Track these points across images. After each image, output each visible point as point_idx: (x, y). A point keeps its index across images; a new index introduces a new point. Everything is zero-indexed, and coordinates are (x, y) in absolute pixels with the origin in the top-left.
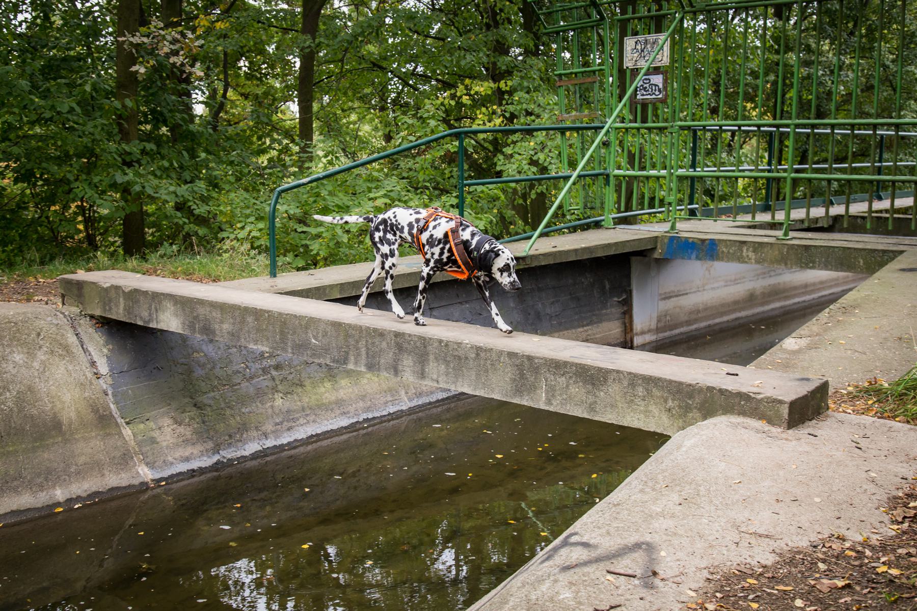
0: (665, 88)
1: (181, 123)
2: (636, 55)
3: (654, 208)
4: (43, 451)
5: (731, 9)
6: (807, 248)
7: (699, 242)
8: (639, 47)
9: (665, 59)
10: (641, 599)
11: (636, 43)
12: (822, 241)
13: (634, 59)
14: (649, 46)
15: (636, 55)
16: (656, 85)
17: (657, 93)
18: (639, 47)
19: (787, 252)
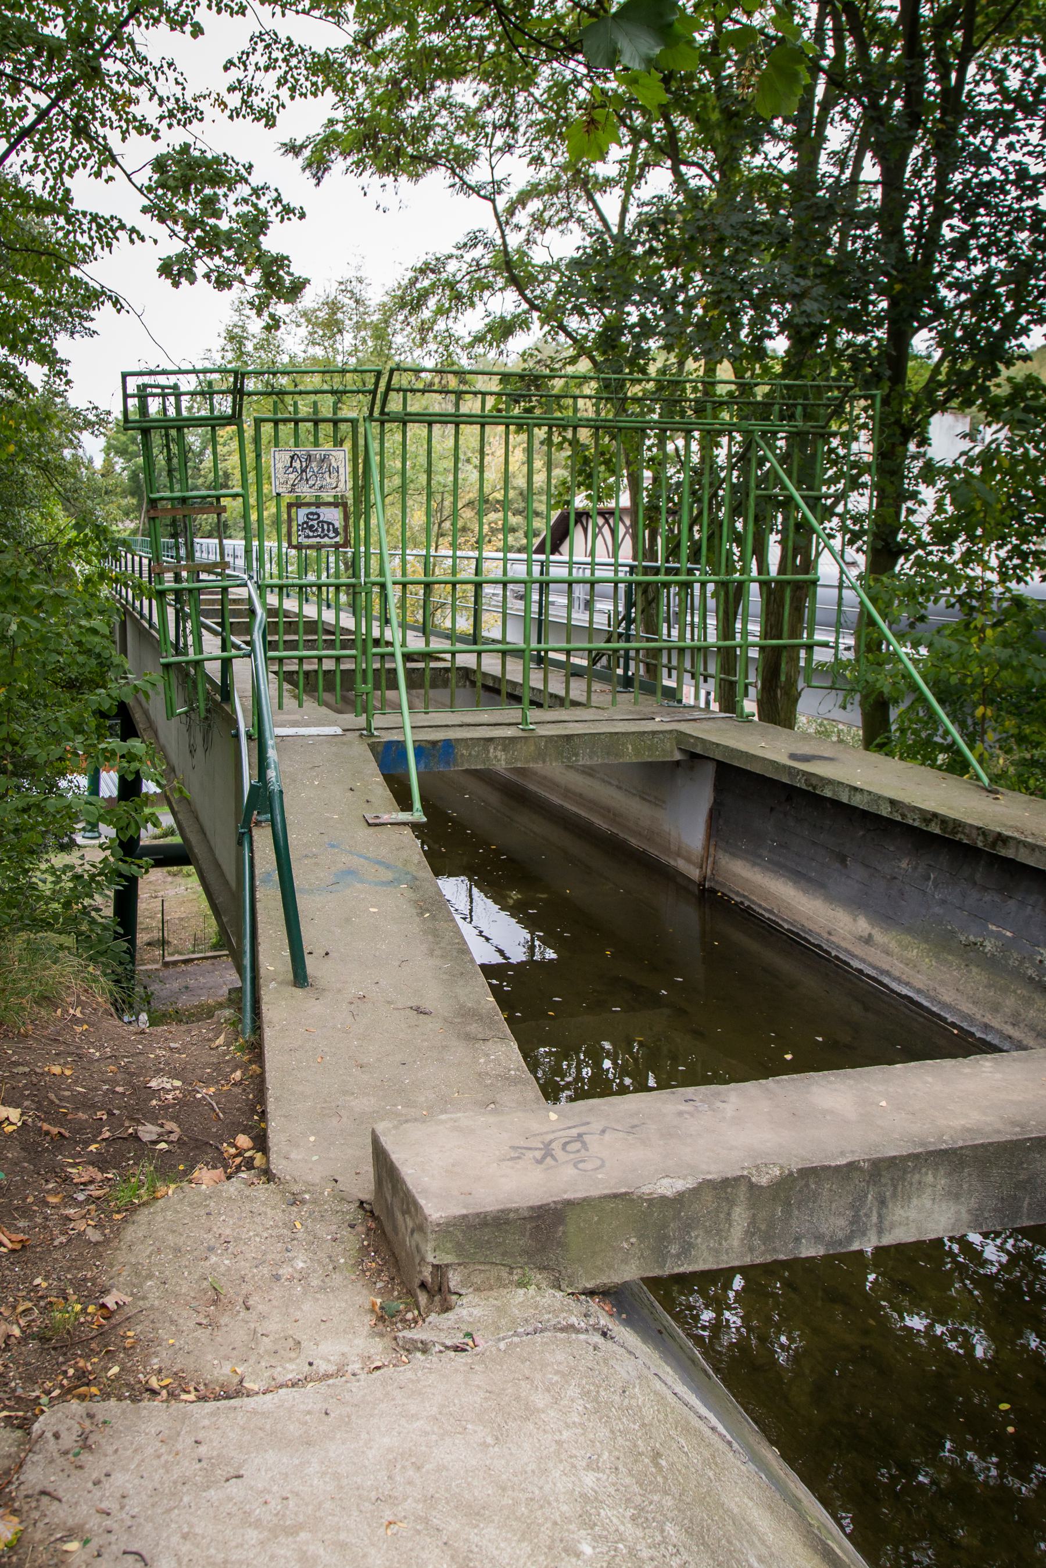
0: (346, 528)
1: (922, 450)
2: (292, 476)
3: (780, 638)
4: (315, 1238)
5: (539, 426)
6: (569, 738)
7: (429, 746)
8: (297, 464)
9: (341, 485)
10: (109, 1532)
11: (292, 458)
12: (587, 725)
13: (290, 482)
14: (314, 464)
15: (292, 476)
16: (329, 523)
17: (332, 534)
18: (297, 464)
19: (546, 746)
